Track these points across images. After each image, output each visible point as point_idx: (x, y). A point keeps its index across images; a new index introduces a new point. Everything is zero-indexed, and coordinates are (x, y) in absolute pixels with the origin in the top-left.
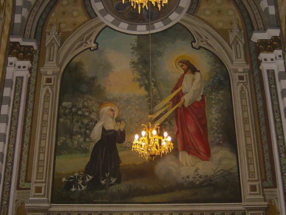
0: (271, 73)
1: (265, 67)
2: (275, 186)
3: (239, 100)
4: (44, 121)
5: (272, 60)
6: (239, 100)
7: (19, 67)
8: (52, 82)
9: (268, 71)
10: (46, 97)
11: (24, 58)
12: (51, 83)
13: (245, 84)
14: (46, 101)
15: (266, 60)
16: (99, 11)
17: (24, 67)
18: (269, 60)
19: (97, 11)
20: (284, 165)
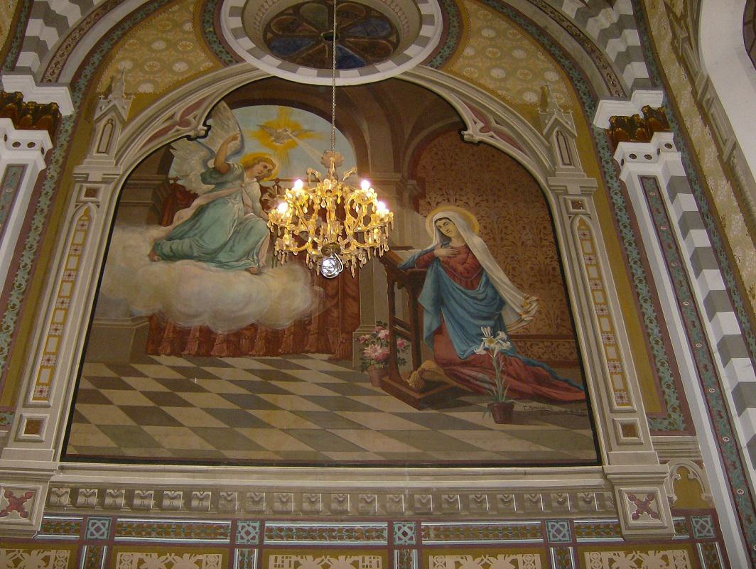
0: (649, 182)
1: (631, 171)
2: (690, 429)
3: (33, 415)
4: (71, 281)
5: (648, 157)
6: (33, 415)
7: (17, 144)
8: (625, 438)
9: (643, 179)
10: (623, 397)
11: (34, 124)
12: (624, 436)
13: (573, 216)
14: (624, 391)
15: (633, 156)
16: (232, 30)
17: (31, 145)
18: (640, 157)
19: (226, 29)
20: (746, 395)
